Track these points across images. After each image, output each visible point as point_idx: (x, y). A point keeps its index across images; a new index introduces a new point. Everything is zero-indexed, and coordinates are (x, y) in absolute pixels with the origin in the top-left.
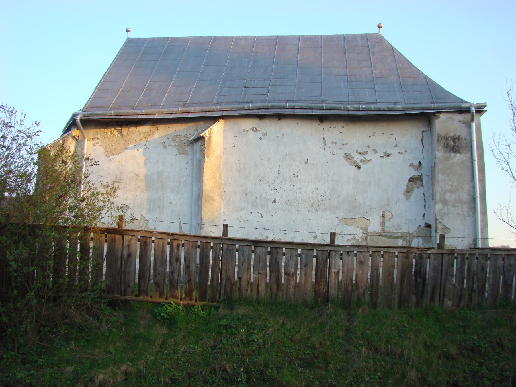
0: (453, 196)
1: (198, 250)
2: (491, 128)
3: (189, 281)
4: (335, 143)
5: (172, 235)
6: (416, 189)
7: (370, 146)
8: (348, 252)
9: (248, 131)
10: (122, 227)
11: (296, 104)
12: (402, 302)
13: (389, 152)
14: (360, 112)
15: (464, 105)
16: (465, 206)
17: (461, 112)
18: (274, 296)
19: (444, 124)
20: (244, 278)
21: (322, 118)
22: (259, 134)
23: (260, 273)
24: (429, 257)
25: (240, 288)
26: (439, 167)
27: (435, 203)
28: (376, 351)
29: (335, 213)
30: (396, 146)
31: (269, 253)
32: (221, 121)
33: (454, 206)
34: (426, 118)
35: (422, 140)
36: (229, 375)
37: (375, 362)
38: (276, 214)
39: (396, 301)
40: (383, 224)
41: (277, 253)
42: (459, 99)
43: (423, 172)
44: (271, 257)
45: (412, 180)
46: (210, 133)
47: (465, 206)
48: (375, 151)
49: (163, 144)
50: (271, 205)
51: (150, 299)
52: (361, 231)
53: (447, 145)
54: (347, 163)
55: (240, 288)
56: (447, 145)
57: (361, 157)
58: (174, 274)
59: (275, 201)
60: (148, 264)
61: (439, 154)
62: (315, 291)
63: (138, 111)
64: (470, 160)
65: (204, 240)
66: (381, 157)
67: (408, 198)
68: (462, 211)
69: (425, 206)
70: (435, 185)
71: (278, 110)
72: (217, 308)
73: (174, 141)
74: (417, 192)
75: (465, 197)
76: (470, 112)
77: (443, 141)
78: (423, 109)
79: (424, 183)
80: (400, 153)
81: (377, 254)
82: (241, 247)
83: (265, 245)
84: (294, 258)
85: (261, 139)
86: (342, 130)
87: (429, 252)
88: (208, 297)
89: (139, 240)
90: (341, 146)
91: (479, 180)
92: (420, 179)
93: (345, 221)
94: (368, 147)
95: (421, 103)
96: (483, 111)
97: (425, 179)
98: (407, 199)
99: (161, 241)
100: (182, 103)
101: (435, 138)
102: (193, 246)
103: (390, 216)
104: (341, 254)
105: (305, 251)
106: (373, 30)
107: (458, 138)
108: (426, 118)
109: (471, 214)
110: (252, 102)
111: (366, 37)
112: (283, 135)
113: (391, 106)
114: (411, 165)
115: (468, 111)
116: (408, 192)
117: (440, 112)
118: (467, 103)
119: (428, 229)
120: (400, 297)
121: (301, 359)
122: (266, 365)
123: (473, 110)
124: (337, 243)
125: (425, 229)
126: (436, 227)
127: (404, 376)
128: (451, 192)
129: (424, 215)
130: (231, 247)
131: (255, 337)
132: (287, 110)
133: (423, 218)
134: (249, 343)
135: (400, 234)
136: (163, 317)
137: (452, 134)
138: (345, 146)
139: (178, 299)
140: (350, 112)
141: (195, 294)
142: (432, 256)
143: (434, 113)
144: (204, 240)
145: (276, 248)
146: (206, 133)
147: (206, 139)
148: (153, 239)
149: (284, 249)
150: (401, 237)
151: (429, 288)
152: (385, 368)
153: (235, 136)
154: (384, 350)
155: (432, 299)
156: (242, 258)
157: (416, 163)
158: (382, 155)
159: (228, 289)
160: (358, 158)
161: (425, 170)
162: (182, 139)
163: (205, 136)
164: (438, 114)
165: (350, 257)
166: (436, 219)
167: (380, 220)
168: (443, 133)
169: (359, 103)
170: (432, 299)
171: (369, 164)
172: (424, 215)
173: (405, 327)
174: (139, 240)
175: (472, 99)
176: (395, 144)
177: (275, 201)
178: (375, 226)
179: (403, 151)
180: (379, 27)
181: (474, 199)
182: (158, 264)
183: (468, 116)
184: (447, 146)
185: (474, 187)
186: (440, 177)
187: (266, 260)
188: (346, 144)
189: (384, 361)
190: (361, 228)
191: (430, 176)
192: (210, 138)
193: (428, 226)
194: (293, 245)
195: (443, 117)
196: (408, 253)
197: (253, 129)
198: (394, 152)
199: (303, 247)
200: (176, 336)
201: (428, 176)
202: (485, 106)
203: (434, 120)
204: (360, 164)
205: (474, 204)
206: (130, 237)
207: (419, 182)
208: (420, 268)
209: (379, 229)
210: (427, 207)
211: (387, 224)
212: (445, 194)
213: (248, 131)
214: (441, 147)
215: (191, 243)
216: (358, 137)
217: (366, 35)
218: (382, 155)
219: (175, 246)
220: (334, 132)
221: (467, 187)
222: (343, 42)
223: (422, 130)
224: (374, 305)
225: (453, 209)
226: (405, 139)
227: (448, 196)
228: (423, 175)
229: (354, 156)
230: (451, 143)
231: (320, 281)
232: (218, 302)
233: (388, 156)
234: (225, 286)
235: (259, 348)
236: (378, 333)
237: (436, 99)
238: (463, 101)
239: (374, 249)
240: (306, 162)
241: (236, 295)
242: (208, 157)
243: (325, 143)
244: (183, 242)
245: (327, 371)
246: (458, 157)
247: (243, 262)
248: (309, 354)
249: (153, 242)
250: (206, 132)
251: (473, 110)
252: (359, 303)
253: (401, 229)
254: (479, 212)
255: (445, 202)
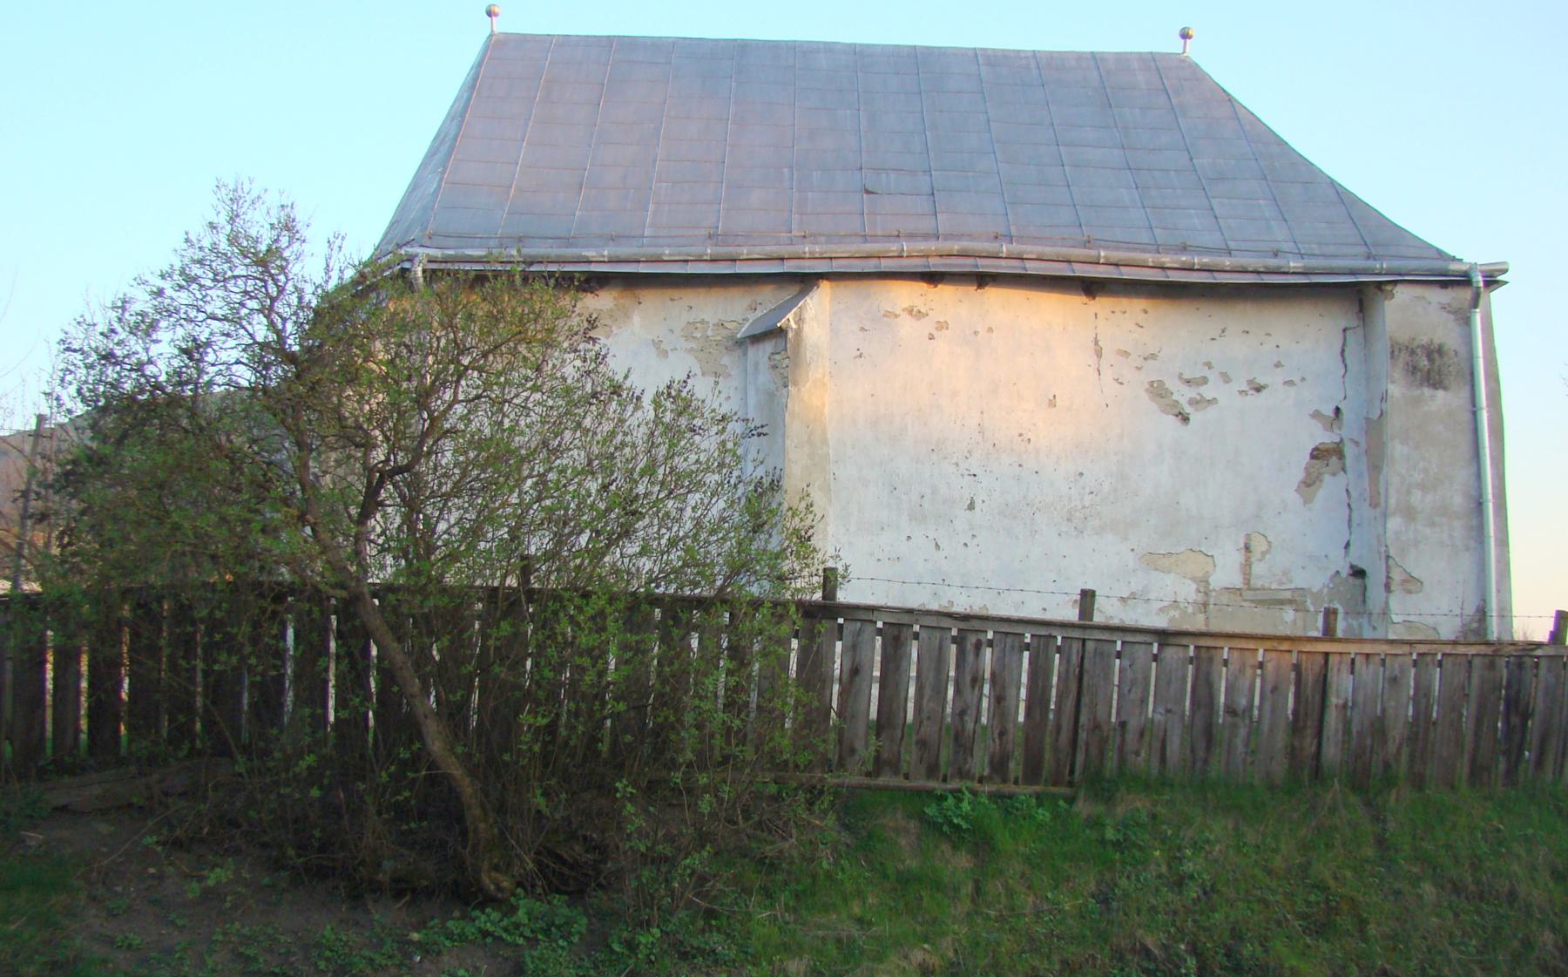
0: (1429, 498)
1: (1026, 654)
2: (1513, 327)
3: (1002, 734)
4: (1126, 354)
5: (966, 618)
6: (1327, 478)
7: (1214, 363)
8: (1368, 655)
9: (896, 316)
10: (833, 596)
11: (1028, 248)
12: (1478, 773)
13: (1261, 381)
14: (1195, 274)
15: (1453, 267)
16: (1457, 524)
17: (1444, 285)
18: (1198, 764)
19: (1408, 313)
20: (1133, 724)
21: (1091, 287)
22: (927, 326)
23: (1168, 711)
24: (1537, 665)
25: (1121, 749)
26: (1394, 423)
27: (1385, 516)
28: (1457, 889)
29: (1126, 539)
30: (1278, 365)
31: (1191, 660)
32: (824, 290)
33: (1433, 524)
34: (1356, 296)
35: (1343, 351)
36: (1155, 960)
37: (1457, 915)
38: (975, 541)
39: (1463, 768)
40: (1247, 566)
41: (1211, 660)
42: (1431, 247)
43: (1345, 433)
44: (1197, 670)
45: (1318, 454)
46: (800, 320)
47: (1457, 524)
48: (1226, 378)
49: (657, 344)
50: (962, 514)
51: (907, 784)
52: (1194, 586)
53: (1415, 368)
54: (1154, 406)
55: (1121, 749)
56: (1415, 368)
57: (1190, 393)
58: (966, 718)
59: (971, 507)
60: (902, 695)
61: (1396, 390)
62: (1293, 753)
63: (590, 253)
64: (1469, 406)
65: (1043, 631)
66: (1241, 392)
67: (1307, 501)
68: (1451, 536)
69: (1350, 521)
70: (1385, 469)
71: (980, 262)
72: (1071, 800)
73: (689, 337)
74: (1331, 487)
75: (1458, 501)
76: (1465, 285)
77: (1403, 357)
78: (1352, 273)
79: (1348, 461)
80: (1290, 383)
81: (1428, 659)
82: (1128, 647)
83: (1185, 641)
84: (1249, 672)
85: (931, 338)
86: (1141, 318)
87: (1539, 652)
88: (1045, 773)
89: (879, 632)
90: (1139, 362)
91: (1492, 458)
92: (1337, 451)
93: (1152, 561)
94: (1209, 365)
95: (1346, 260)
96: (1497, 282)
97: (1349, 450)
98: (1305, 502)
99: (937, 634)
100: (703, 232)
101: (1381, 349)
102: (1013, 647)
103: (1264, 547)
104: (1353, 661)
105: (1273, 655)
106: (1174, 46)
107: (1440, 351)
108: (1356, 296)
109: (1472, 544)
110: (912, 236)
111: (1153, 63)
112: (990, 330)
113: (1273, 262)
114: (1316, 415)
115: (1464, 280)
116: (1309, 483)
117: (1395, 282)
118: (1454, 259)
119: (1358, 581)
120: (1473, 760)
121: (1305, 916)
122: (1237, 935)
123: (1479, 280)
124: (1098, 619)
125: (1351, 579)
126: (1388, 577)
127: (1527, 943)
128: (1423, 487)
129: (1347, 545)
130: (1106, 647)
131: (1188, 867)
132: (1003, 262)
133: (1347, 553)
134: (1179, 883)
135: (1288, 595)
136: (958, 827)
137: (1424, 340)
138: (1150, 362)
139: (973, 779)
140: (1170, 273)
141: (1015, 767)
142: (1543, 663)
143: (1379, 285)
144: (1043, 631)
145: (1208, 648)
146: (789, 320)
147: (790, 335)
148: (916, 628)
149: (1261, 651)
150: (1290, 602)
151: (1533, 737)
152: (1484, 928)
153: (862, 329)
154: (1472, 888)
155: (1539, 763)
156: (1129, 675)
157: (1330, 412)
158: (1244, 387)
159: (1094, 750)
160: (1182, 395)
161: (1351, 428)
162: (709, 333)
163: (788, 326)
164: (1389, 288)
165: (1371, 667)
166: (1388, 557)
167: (1239, 557)
168: (1403, 337)
169: (1184, 249)
170: (1539, 763)
171: (1211, 412)
172: (1347, 545)
173: (1499, 830)
174: (879, 632)
175: (1470, 252)
176: (1275, 360)
177: (971, 507)
178: (1226, 574)
179: (1296, 379)
180: (1185, 35)
181: (1479, 505)
182: (928, 692)
183: (1465, 294)
184: (1413, 370)
185: (1479, 476)
186: (1397, 450)
187: (1184, 678)
188: (1153, 356)
189: (1479, 912)
190: (1194, 579)
191: (1363, 445)
192: (799, 332)
193: (1359, 573)
194: (1009, 628)
195: (1402, 294)
196: (1495, 655)
197: (910, 312)
198: (1274, 379)
199: (1268, 644)
200: (1001, 872)
201: (1357, 443)
202: (1504, 271)
203: (1373, 303)
204: (1188, 409)
205: (1479, 519)
206: (859, 624)
207: (1334, 459)
208: (1519, 692)
209: (1237, 581)
210: (1354, 524)
211: (1258, 568)
212: (1409, 492)
213: (896, 316)
214: (1398, 374)
215: (1009, 640)
216: (1180, 336)
217: (1153, 57)
218: (1244, 387)
219: (969, 647)
220: (1120, 321)
221: (1462, 475)
222: (1095, 74)
223: (1343, 324)
224: (1418, 782)
225: (1428, 531)
226: (1304, 342)
227: (1416, 497)
228: (1346, 442)
229: (1172, 388)
230: (1424, 362)
231: (1305, 727)
232: (1071, 784)
233: (1258, 389)
234: (1087, 744)
235: (1205, 893)
236: (1449, 847)
237: (1375, 245)
238: (1440, 254)
239: (1422, 649)
240: (1052, 403)
241: (1111, 763)
242: (795, 384)
243: (1099, 354)
244: (990, 635)
245: (1365, 939)
246: (1440, 400)
247: (1133, 683)
248: (1318, 903)
249: (916, 636)
250: (790, 316)
251: (1479, 280)
252: (1389, 782)
253: (1291, 582)
254: (1492, 541)
255: (1410, 514)
